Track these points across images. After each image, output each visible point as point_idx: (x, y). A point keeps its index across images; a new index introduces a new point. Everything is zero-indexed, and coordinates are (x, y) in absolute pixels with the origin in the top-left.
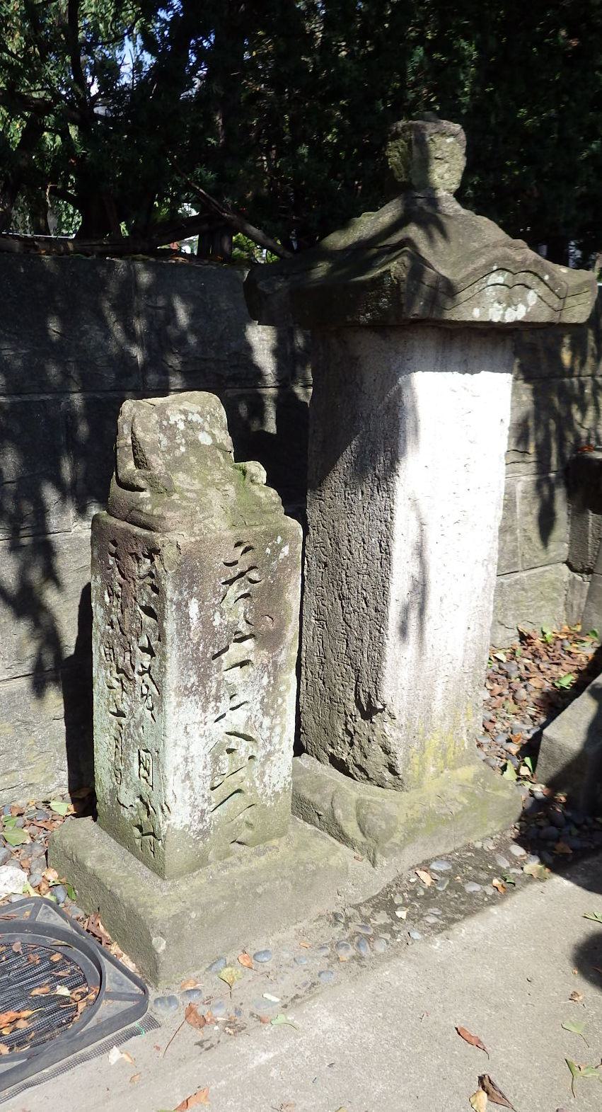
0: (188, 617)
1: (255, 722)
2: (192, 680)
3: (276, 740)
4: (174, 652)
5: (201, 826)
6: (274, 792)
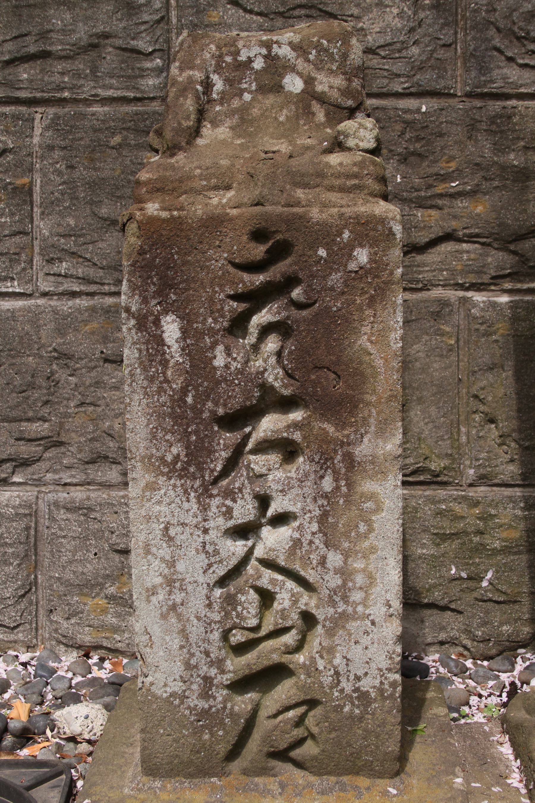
0: (160, 341)
1: (309, 552)
2: (175, 450)
3: (357, 596)
4: (136, 397)
5: (203, 704)
6: (356, 690)
